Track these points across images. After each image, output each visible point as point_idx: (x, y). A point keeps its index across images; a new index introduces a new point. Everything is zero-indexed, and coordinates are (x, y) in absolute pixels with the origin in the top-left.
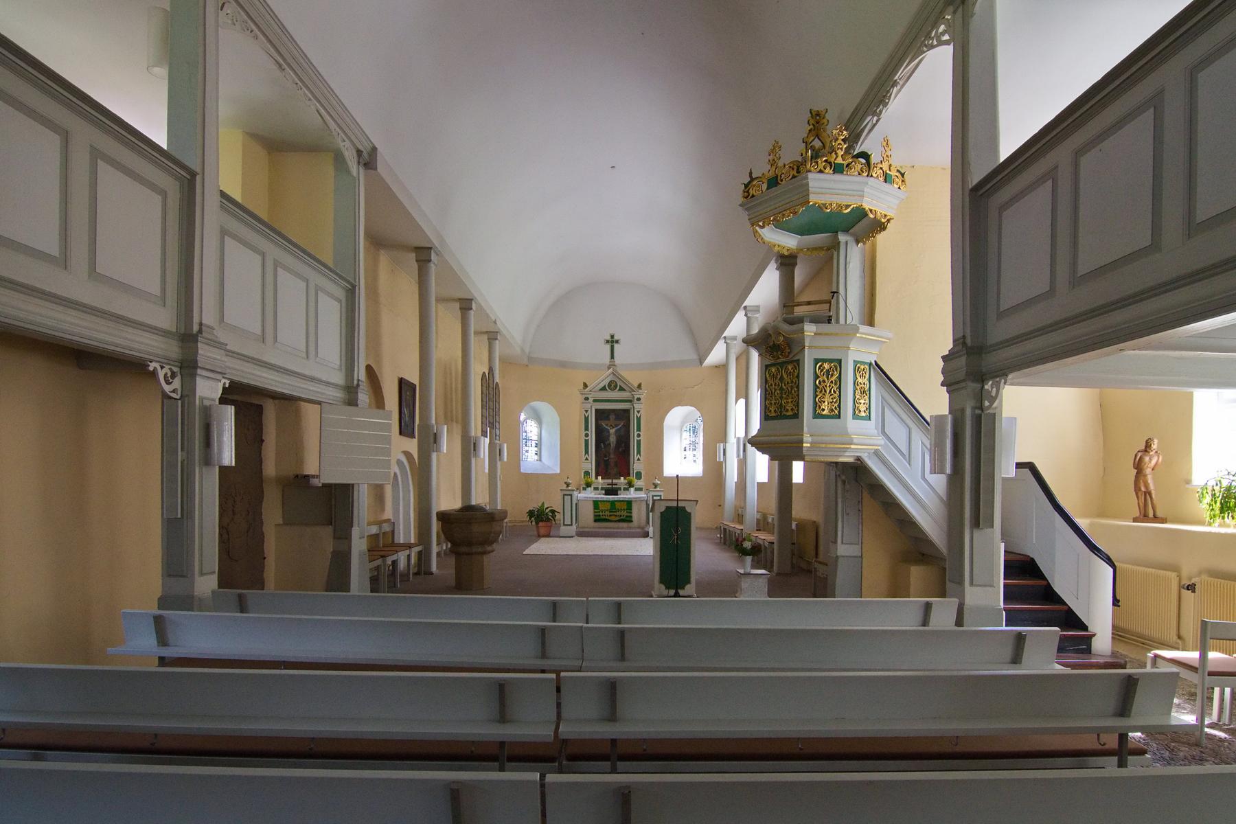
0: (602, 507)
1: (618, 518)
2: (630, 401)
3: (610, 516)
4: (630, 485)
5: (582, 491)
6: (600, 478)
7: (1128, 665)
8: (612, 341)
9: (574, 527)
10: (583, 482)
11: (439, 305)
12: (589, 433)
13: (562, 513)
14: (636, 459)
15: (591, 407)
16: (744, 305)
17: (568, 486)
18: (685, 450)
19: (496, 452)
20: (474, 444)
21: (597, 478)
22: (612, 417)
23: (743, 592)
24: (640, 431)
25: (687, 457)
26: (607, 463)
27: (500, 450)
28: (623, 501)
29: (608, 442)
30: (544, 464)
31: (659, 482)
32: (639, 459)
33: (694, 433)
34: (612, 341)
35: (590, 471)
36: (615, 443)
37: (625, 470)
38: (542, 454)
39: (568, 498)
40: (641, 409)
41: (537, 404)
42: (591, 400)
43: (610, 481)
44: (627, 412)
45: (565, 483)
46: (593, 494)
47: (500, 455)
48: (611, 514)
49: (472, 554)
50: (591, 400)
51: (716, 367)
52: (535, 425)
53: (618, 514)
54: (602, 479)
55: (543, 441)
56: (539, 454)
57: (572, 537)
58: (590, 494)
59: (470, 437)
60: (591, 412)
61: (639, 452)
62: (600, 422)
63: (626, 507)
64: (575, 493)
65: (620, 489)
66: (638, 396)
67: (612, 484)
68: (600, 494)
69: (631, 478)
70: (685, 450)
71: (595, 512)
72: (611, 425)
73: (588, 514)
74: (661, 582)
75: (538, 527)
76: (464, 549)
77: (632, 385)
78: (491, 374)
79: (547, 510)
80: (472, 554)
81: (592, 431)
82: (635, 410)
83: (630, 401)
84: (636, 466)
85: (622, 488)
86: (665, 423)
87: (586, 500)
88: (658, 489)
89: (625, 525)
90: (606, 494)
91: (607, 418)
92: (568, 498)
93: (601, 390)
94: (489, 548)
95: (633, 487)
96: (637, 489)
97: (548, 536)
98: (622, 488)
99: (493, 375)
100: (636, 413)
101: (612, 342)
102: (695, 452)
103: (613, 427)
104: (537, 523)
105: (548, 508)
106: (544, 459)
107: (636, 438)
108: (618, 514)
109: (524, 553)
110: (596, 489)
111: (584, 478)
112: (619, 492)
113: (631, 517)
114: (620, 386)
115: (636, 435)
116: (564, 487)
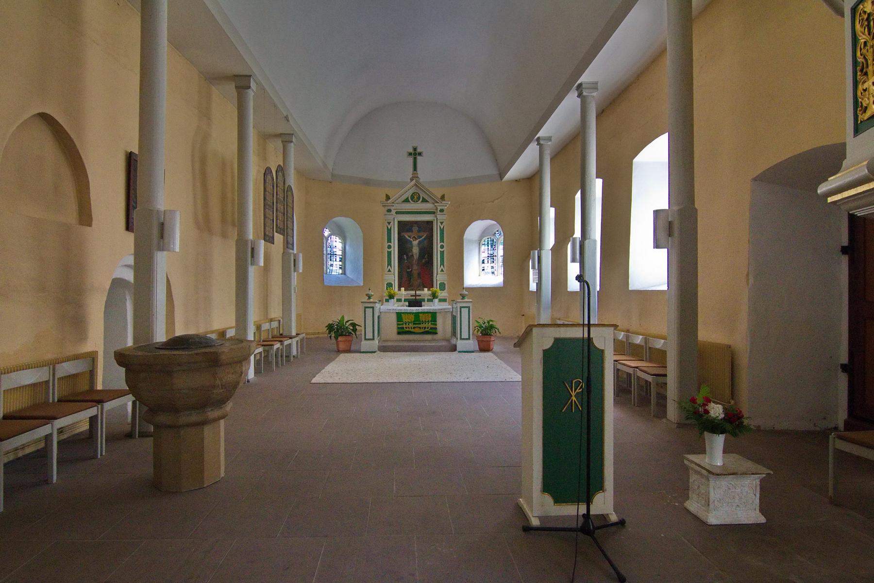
0: (405, 319)
1: (422, 330)
2: (434, 213)
3: (414, 328)
4: (434, 296)
5: (385, 303)
6: (403, 289)
7: (426, 305)
8: (415, 154)
9: (376, 341)
10: (386, 294)
11: (213, 88)
12: (392, 245)
13: (363, 326)
14: (439, 270)
15: (394, 219)
16: (579, 82)
17: (369, 298)
18: (483, 263)
19: (290, 262)
20: (253, 249)
21: (399, 290)
22: (415, 229)
23: (711, 506)
24: (443, 242)
25: (485, 268)
26: (410, 274)
27: (295, 260)
28: (428, 313)
29: (411, 254)
30: (348, 277)
31: (372, 294)
32: (442, 271)
33: (492, 246)
34: (415, 154)
35: (393, 283)
36: (418, 254)
37: (427, 281)
38: (347, 267)
39: (369, 311)
40: (440, 222)
41: (341, 220)
42: (393, 212)
43: (413, 292)
44: (430, 224)
45: (367, 295)
46: (396, 305)
47: (295, 266)
48: (415, 326)
49: (179, 427)
50: (393, 212)
51: (516, 181)
52: (340, 241)
53: (421, 326)
54: (405, 290)
55: (347, 255)
56: (343, 268)
57: (375, 352)
58: (394, 306)
59: (247, 241)
60: (394, 225)
61: (442, 263)
62: (402, 234)
63: (430, 319)
64: (378, 306)
65: (424, 300)
66: (441, 208)
67: (416, 295)
68: (403, 306)
69: (434, 289)
70: (483, 263)
71: (398, 324)
72: (414, 237)
73: (390, 326)
74: (547, 488)
75: (337, 342)
76: (164, 418)
77: (435, 196)
78: (280, 174)
79: (348, 324)
80: (179, 427)
81: (394, 244)
82: (439, 221)
83: (434, 213)
84: (440, 276)
85: (426, 300)
86: (464, 237)
87: (388, 312)
88: (466, 300)
89: (429, 337)
90: (409, 306)
91: (410, 230)
92: (369, 311)
93: (404, 201)
94: (212, 414)
95: (437, 298)
96: (440, 300)
97: (349, 351)
98: (426, 300)
99: (284, 175)
100: (439, 224)
101: (415, 154)
102: (492, 265)
103: (416, 239)
104: (336, 338)
105: (347, 322)
106: (348, 272)
107: (439, 249)
108: (421, 326)
109: (314, 381)
110: (399, 300)
111: (387, 289)
112: (423, 303)
113: (436, 328)
114: (423, 198)
115: (439, 246)
116: (365, 299)
